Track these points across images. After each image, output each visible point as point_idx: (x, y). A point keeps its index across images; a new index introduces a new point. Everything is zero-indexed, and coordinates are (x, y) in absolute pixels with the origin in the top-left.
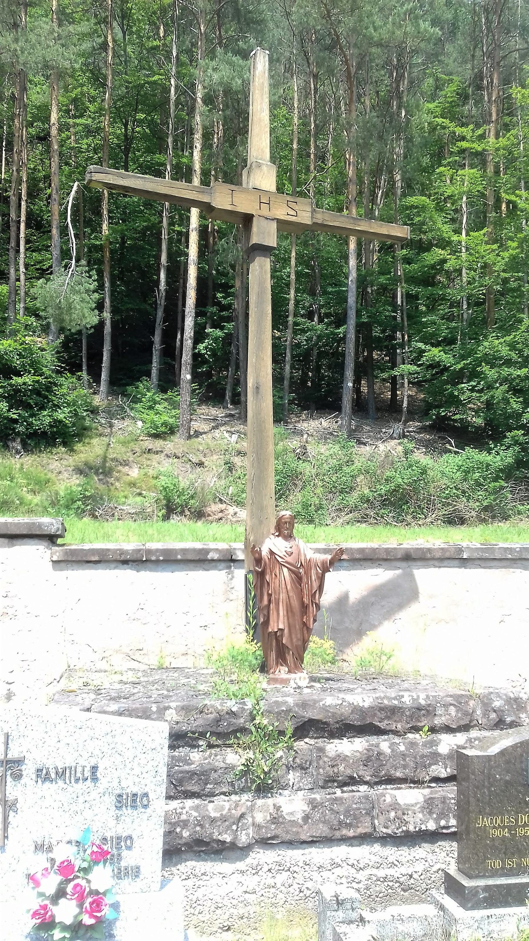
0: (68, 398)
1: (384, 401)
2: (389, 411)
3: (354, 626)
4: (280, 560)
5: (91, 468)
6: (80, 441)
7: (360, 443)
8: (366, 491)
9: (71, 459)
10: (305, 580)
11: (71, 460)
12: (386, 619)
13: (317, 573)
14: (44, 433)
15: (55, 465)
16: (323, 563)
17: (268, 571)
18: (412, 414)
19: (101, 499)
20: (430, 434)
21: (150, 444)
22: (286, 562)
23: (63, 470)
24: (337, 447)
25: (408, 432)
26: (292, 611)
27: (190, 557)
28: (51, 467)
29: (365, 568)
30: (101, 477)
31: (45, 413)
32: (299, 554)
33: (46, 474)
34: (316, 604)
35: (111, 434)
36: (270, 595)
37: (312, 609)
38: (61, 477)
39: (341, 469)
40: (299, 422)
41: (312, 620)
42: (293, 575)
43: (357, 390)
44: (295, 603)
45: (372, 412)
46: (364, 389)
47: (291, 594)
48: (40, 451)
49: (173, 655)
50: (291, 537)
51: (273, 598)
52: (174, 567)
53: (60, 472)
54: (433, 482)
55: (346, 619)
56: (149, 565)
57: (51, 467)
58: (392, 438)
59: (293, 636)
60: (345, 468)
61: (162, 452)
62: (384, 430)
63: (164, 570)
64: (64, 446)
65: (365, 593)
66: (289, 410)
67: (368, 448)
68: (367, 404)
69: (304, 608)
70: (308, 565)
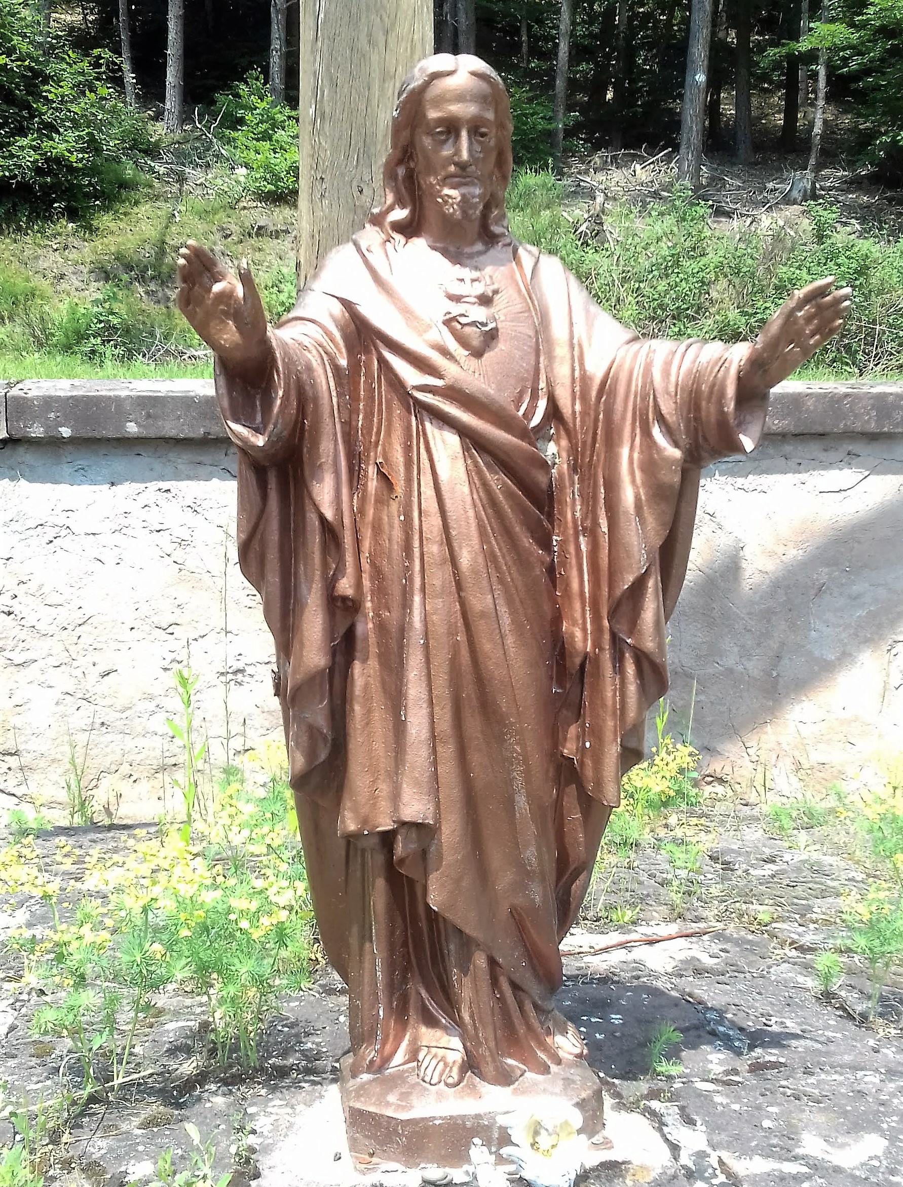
0: (74, 108)
1: (765, 132)
2: (785, 148)
3: (754, 667)
4: (410, 376)
5: (129, 268)
6: (106, 209)
7: (719, 212)
8: (733, 314)
9: (87, 248)
10: (572, 509)
11: (87, 251)
12: (867, 641)
13: (651, 464)
14: (25, 188)
15: (51, 261)
16: (694, 398)
17: (330, 447)
18: (828, 157)
19: (152, 334)
20: (871, 194)
21: (261, 215)
22: (454, 393)
23: (69, 270)
24: (670, 221)
25: (822, 189)
26: (487, 707)
27: (170, 429)
28: (42, 264)
29: (799, 468)
30: (153, 287)
31: (24, 142)
32: (540, 341)
33: (28, 280)
34: (641, 657)
35: (178, 197)
36: (342, 610)
37: (618, 687)
38: (64, 285)
39: (677, 264)
40: (586, 172)
41: (612, 751)
42: (497, 480)
43: (712, 110)
44: (512, 659)
45: (743, 150)
46: (728, 110)
47: (481, 600)
48: (19, 229)
49: (125, 769)
50: (489, 238)
51: (366, 627)
52: (119, 464)
53: (62, 276)
54: (880, 292)
55: (727, 644)
56: (23, 454)
57: (42, 264)
58: (788, 200)
59: (496, 857)
60: (686, 263)
61: (287, 232)
62: (770, 185)
63: (82, 476)
64: (71, 219)
65: (794, 554)
66: (565, 151)
67: (735, 223)
68: (734, 137)
69: (567, 680)
70: (596, 420)
